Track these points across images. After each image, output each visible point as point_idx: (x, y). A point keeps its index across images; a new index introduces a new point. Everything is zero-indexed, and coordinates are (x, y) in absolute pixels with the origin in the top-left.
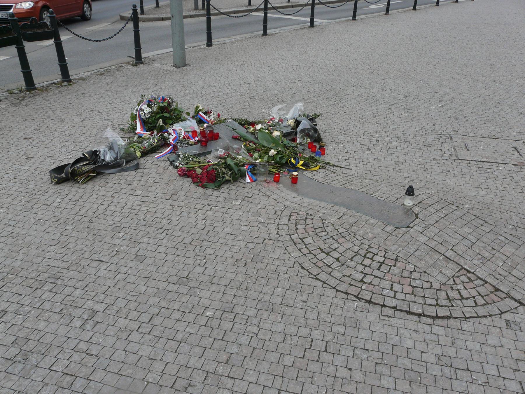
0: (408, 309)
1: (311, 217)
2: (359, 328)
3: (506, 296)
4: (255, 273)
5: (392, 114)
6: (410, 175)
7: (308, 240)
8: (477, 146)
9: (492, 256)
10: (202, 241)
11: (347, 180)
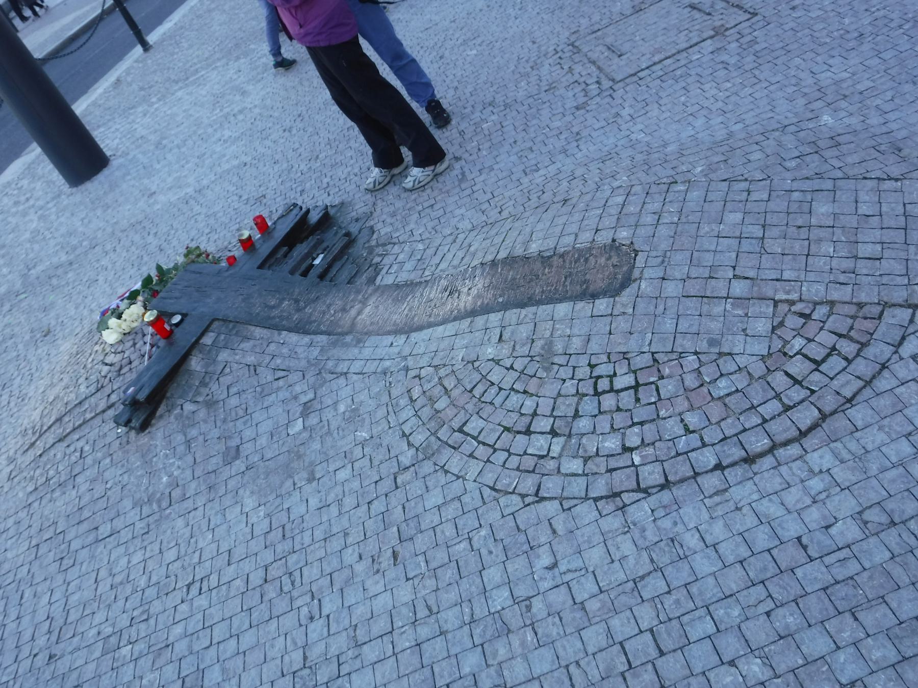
0: (743, 454)
1: (448, 370)
2: (686, 557)
3: (880, 308)
4: (423, 564)
5: (452, 65)
6: (559, 165)
7: (473, 426)
8: (628, 38)
9: (806, 243)
10: (284, 560)
11: (460, 248)
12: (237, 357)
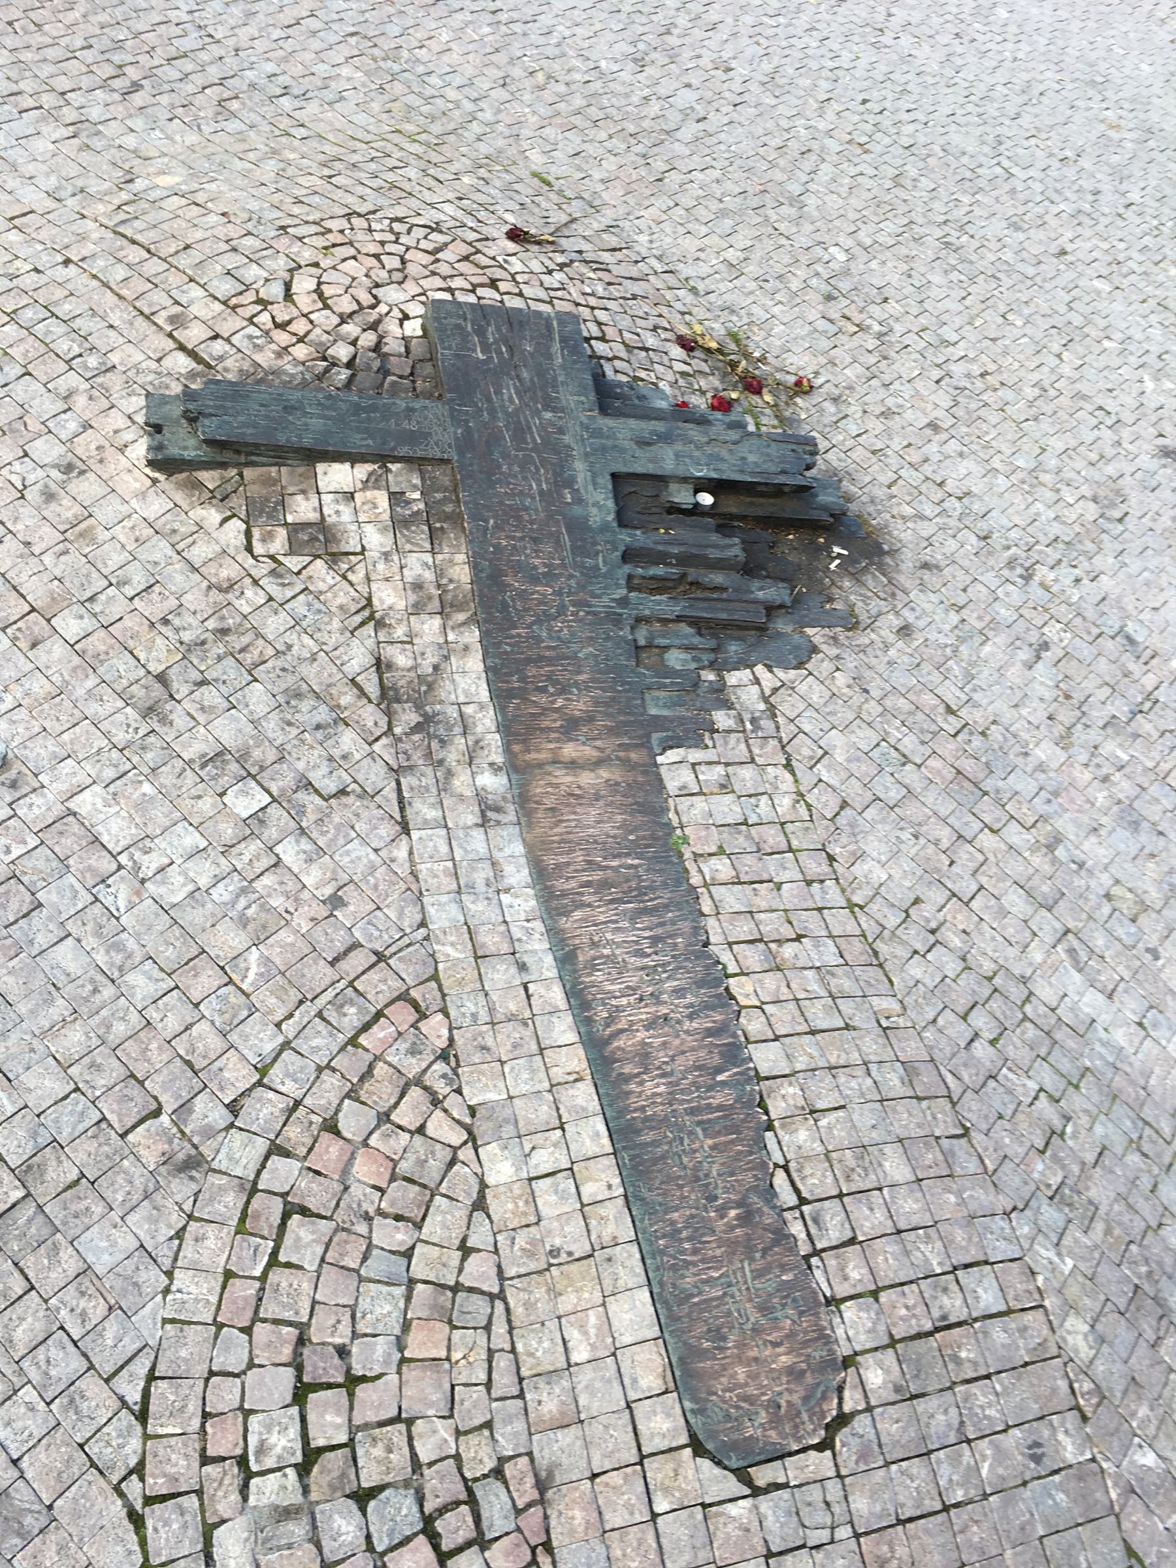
12: (381, 566)
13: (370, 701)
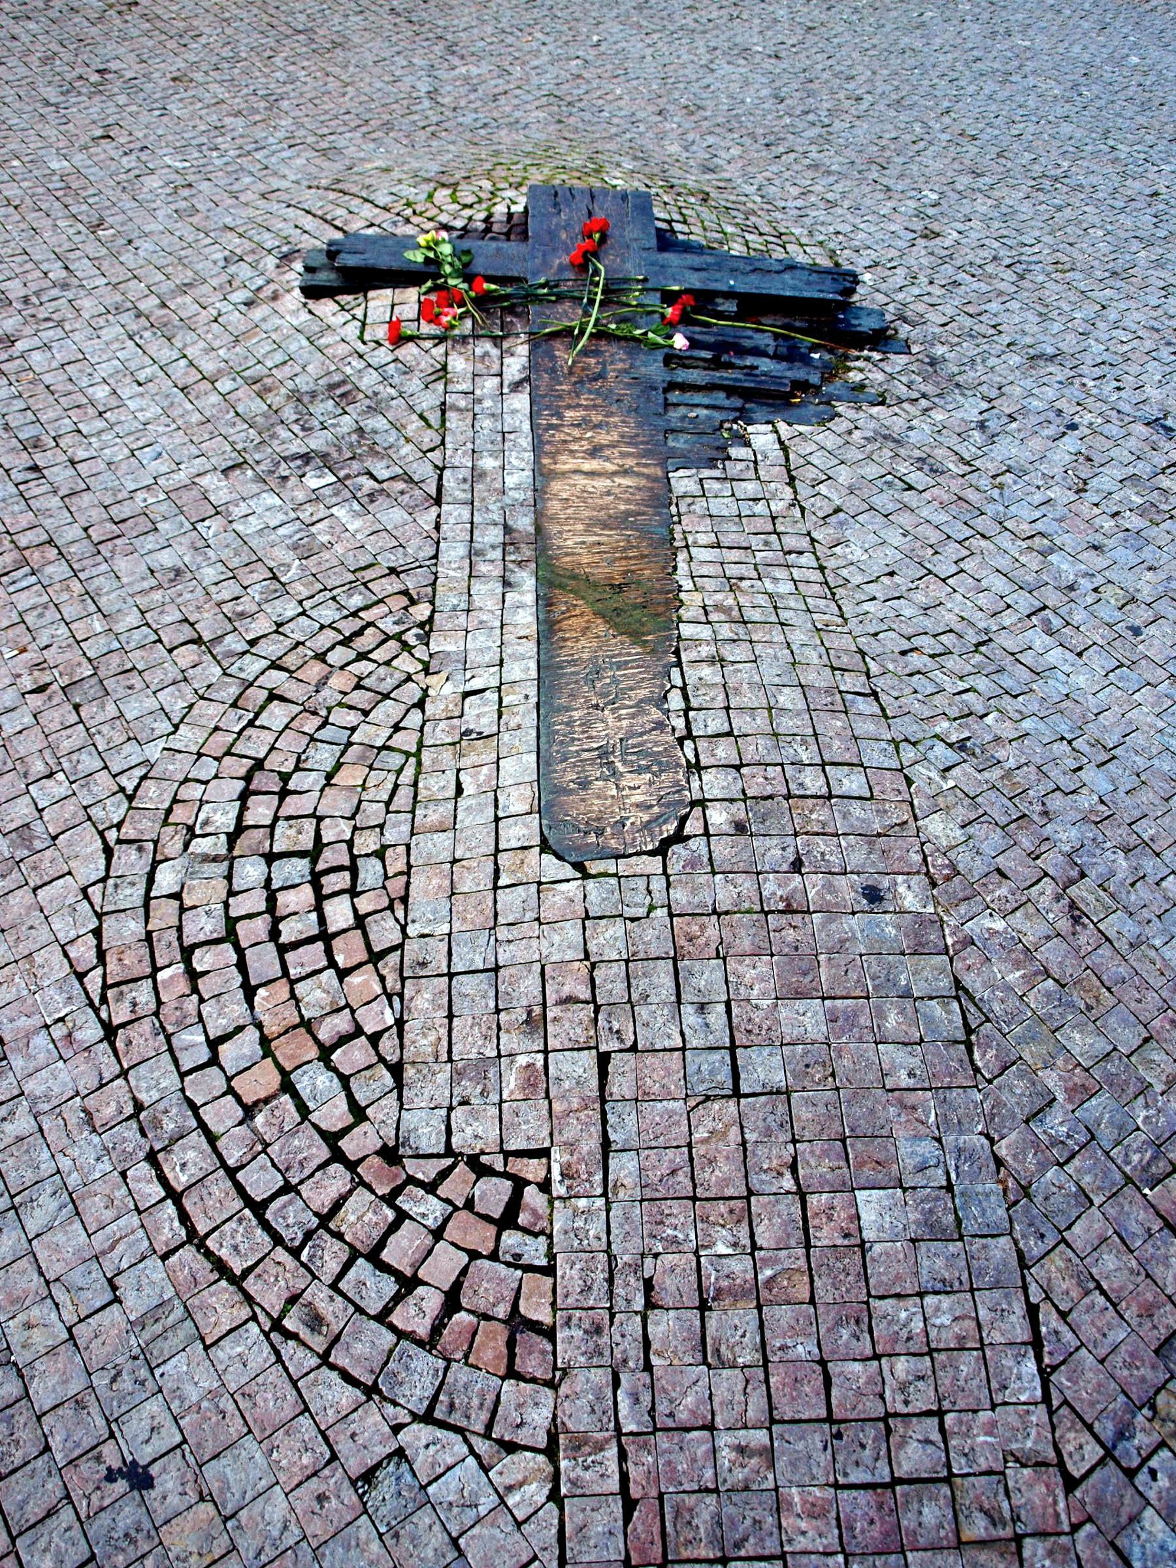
13: (429, 426)
